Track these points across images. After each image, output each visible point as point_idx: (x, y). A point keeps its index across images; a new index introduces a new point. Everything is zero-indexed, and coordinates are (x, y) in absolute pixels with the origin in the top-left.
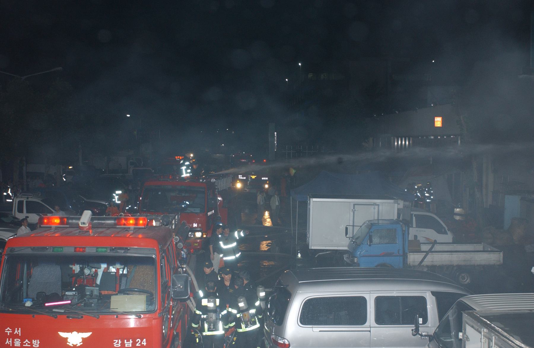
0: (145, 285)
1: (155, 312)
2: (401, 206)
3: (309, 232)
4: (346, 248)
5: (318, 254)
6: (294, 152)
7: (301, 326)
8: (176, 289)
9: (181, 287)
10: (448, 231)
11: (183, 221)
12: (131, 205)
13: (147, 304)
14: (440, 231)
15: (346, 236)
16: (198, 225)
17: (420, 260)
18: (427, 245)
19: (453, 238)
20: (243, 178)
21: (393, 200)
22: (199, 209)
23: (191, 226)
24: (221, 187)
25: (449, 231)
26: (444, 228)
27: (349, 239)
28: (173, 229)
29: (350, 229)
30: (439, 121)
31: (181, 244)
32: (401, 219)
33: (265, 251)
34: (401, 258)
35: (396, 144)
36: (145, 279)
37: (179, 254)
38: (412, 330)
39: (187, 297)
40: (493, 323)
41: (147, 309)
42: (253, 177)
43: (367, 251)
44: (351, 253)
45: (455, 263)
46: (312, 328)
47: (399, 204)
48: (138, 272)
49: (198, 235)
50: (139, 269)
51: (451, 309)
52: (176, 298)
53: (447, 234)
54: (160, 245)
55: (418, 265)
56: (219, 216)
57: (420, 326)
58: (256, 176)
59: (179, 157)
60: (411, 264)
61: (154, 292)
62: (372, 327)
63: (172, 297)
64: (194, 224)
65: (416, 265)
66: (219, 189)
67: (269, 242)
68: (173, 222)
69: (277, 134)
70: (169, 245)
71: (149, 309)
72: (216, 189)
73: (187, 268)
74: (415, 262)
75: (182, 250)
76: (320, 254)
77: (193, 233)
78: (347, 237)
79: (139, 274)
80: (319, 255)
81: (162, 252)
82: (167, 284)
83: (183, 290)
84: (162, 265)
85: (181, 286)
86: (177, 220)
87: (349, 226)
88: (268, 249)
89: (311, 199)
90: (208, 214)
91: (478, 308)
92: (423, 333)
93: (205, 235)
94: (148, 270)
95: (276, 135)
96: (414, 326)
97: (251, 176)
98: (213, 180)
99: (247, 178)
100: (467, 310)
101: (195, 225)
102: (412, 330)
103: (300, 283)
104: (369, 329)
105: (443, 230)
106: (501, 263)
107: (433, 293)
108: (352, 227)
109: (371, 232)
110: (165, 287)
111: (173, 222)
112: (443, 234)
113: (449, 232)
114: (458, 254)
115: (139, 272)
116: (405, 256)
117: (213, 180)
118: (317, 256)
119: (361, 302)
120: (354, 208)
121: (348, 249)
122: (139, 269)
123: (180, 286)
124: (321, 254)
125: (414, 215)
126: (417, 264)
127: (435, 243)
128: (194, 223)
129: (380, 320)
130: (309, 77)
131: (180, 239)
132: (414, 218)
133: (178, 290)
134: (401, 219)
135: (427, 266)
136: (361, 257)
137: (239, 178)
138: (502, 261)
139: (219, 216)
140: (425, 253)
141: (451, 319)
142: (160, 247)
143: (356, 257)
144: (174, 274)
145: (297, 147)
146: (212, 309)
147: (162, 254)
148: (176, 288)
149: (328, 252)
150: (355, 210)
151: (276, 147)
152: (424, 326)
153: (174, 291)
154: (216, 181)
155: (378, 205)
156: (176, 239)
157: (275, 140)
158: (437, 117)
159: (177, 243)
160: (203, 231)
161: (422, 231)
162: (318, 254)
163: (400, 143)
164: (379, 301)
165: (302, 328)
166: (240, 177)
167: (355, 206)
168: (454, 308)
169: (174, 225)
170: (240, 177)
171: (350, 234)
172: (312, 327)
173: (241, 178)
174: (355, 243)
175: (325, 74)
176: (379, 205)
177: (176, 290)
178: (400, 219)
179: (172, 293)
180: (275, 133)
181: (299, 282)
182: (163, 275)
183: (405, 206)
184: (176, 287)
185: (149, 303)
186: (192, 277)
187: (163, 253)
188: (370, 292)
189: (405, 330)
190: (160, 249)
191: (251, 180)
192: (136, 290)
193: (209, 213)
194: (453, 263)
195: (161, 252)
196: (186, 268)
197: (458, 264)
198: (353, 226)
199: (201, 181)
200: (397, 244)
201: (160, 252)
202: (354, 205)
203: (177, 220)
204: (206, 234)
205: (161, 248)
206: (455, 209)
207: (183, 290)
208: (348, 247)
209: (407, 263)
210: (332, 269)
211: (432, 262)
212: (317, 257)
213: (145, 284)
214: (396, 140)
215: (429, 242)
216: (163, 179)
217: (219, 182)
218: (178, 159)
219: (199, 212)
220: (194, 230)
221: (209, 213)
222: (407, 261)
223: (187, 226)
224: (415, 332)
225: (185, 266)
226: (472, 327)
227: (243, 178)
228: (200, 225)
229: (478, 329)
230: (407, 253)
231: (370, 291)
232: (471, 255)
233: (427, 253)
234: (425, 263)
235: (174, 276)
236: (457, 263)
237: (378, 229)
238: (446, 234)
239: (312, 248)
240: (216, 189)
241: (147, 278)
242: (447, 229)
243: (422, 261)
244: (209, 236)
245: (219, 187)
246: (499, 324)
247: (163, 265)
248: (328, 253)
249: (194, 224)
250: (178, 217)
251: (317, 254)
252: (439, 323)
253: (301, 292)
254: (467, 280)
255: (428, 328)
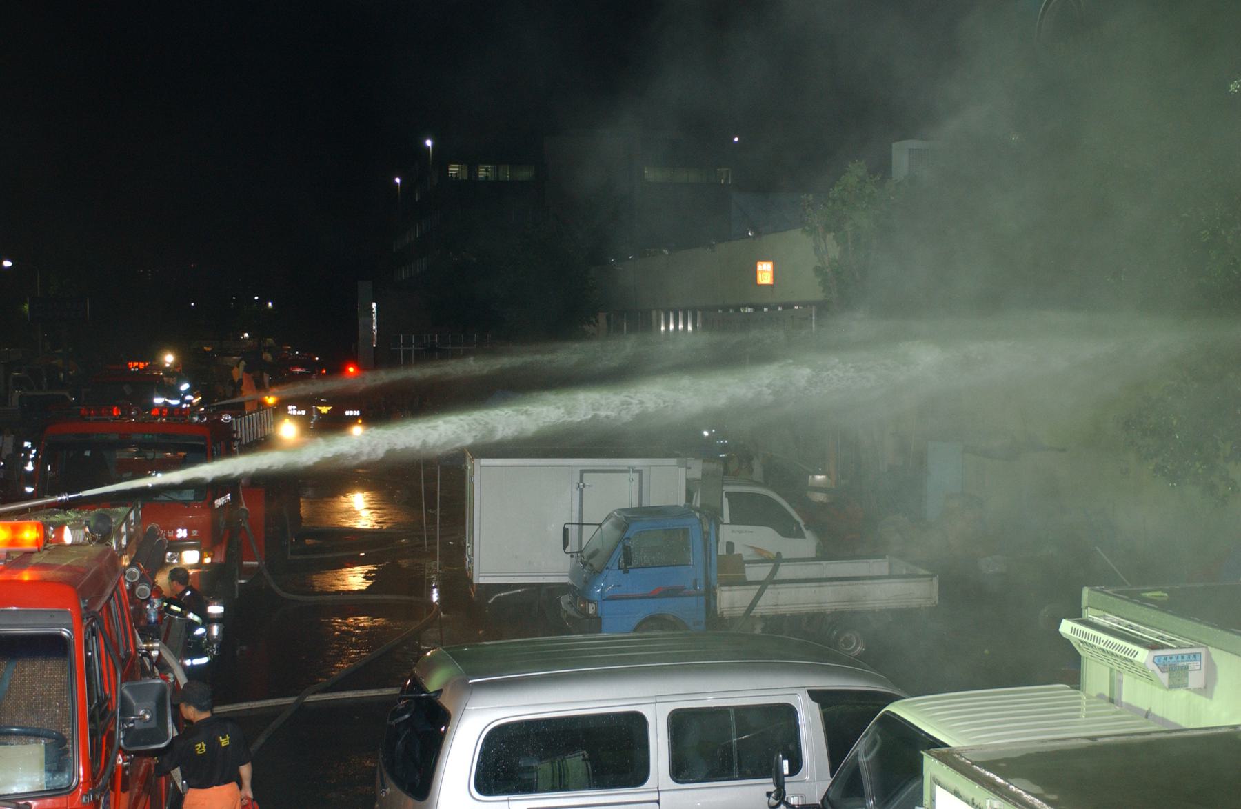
0: (44, 713)
1: (71, 792)
2: (696, 473)
3: (471, 542)
4: (566, 580)
5: (496, 596)
6: (420, 348)
7: (480, 799)
8: (131, 725)
9: (148, 717)
10: (807, 529)
11: (149, 527)
12: (23, 490)
13: (48, 770)
14: (788, 529)
15: (564, 548)
16: (189, 533)
17: (748, 603)
18: (760, 564)
19: (818, 548)
20: (299, 413)
21: (675, 460)
22: (193, 491)
23: (170, 534)
24: (252, 428)
25: (809, 531)
26: (798, 523)
27: (572, 556)
28: (123, 547)
29: (574, 531)
30: (767, 272)
31: (144, 587)
32: (697, 502)
33: (360, 591)
34: (702, 599)
35: (663, 328)
36: (42, 695)
37: (139, 613)
38: (769, 794)
39: (163, 745)
40: (1011, 781)
41: (47, 783)
42: (325, 410)
43: (619, 586)
44: (578, 591)
45: (829, 608)
46: (507, 803)
47: (690, 468)
48: (21, 675)
49: (190, 557)
50: (24, 667)
51: (864, 736)
52: (132, 749)
53: (805, 537)
54: (84, 599)
55: (744, 614)
56: (244, 507)
57: (786, 779)
58: (330, 408)
59: (136, 364)
60: (725, 613)
61: (68, 732)
62: (655, 791)
63: (120, 748)
64: (179, 531)
65: (739, 617)
66: (241, 440)
67: (371, 567)
68: (124, 529)
69: (377, 307)
70: (111, 596)
71: (51, 786)
72: (235, 439)
73: (162, 651)
74: (734, 607)
75: (148, 601)
76: (499, 595)
77: (176, 552)
78: (566, 551)
79: (25, 680)
80: (499, 597)
81: (90, 619)
82: (106, 705)
83: (153, 724)
84: (90, 654)
85: (146, 713)
86: (133, 524)
87: (571, 524)
88: (368, 587)
89: (476, 460)
90: (214, 505)
91: (929, 725)
92: (792, 799)
93: (209, 556)
94: (51, 670)
95: (375, 310)
96: (771, 780)
97: (319, 408)
98: (226, 418)
99: (309, 415)
100: (934, 748)
101: (182, 533)
102: (769, 794)
103: (471, 683)
104: (655, 797)
105: (794, 528)
106: (935, 603)
107: (815, 695)
108: (584, 523)
109: (629, 539)
110: (100, 715)
111: (124, 529)
112: (795, 537)
113: (807, 533)
114: (834, 586)
115: (25, 676)
116: (709, 595)
117: (226, 418)
118: (492, 599)
119: (633, 725)
120: (581, 480)
121: (571, 582)
122: (24, 667)
123: (143, 716)
124: (502, 594)
125: (726, 493)
126: (739, 612)
127: (777, 560)
128: (179, 528)
129: (681, 771)
130: (451, 174)
131: (142, 576)
132: (726, 501)
133: (138, 725)
134: (697, 502)
135: (764, 618)
136: (604, 600)
137: (290, 412)
138: (937, 598)
139: (244, 507)
140: (758, 587)
141: (862, 760)
142: (83, 606)
143: (592, 602)
144: (124, 679)
145: (427, 337)
146: (216, 617)
147: (90, 624)
148: (133, 722)
149: (519, 591)
150: (584, 486)
151: (375, 338)
152: (794, 780)
153: (128, 731)
154: (234, 419)
155: (640, 472)
156: (132, 575)
157: (372, 321)
158: (761, 261)
159: (133, 586)
160: (202, 549)
161: (746, 532)
162: (496, 596)
163: (672, 327)
164: (680, 722)
165: (481, 803)
166: (293, 409)
167: (585, 474)
168: (869, 735)
169: (125, 537)
170: (293, 409)
171: (573, 546)
172: (508, 801)
173: (295, 412)
174: (588, 567)
175: (489, 166)
176: (641, 470)
177: (132, 727)
178: (692, 503)
179: (122, 737)
180: (374, 305)
181: (471, 681)
182: (94, 683)
183: (705, 474)
184: (133, 717)
185: (55, 766)
186: (176, 673)
187: (93, 620)
188: (655, 700)
189: (757, 790)
190: (84, 612)
191: (318, 417)
192: (15, 730)
193: (219, 502)
194: (823, 608)
195: (85, 620)
196: (159, 650)
197: (836, 609)
198: (581, 524)
199: (196, 419)
200: (691, 567)
201: (83, 619)
202: (582, 472)
203: (133, 524)
204: (212, 554)
205: (86, 608)
206: (810, 477)
207: (153, 724)
208: (572, 576)
209: (716, 611)
210: (549, 641)
211: (775, 606)
212: (494, 601)
213: (42, 708)
214: (662, 317)
215: (763, 558)
216: (95, 417)
217: (241, 422)
218: (134, 368)
219: (192, 499)
220: (179, 546)
221: (219, 502)
222: (715, 607)
223: (160, 539)
224: (776, 799)
225: (157, 645)
226: (956, 794)
227: (299, 413)
228: (195, 533)
229: (973, 799)
230: (715, 588)
231: (656, 696)
232: (865, 586)
233: (763, 584)
234: (759, 610)
235: (125, 685)
236: (834, 608)
237: (641, 532)
238: (800, 538)
239: (481, 582)
240: (235, 439)
241: (49, 691)
242: (805, 526)
243: (753, 605)
244: (218, 560)
245: (241, 435)
246: (1026, 783)
247: (93, 654)
248: (518, 593)
249: (179, 531)
250: (136, 515)
251: (494, 595)
252: (833, 771)
253: (473, 708)
254: (857, 644)
255: (802, 784)
